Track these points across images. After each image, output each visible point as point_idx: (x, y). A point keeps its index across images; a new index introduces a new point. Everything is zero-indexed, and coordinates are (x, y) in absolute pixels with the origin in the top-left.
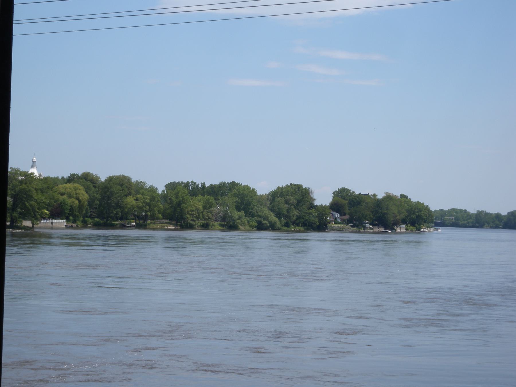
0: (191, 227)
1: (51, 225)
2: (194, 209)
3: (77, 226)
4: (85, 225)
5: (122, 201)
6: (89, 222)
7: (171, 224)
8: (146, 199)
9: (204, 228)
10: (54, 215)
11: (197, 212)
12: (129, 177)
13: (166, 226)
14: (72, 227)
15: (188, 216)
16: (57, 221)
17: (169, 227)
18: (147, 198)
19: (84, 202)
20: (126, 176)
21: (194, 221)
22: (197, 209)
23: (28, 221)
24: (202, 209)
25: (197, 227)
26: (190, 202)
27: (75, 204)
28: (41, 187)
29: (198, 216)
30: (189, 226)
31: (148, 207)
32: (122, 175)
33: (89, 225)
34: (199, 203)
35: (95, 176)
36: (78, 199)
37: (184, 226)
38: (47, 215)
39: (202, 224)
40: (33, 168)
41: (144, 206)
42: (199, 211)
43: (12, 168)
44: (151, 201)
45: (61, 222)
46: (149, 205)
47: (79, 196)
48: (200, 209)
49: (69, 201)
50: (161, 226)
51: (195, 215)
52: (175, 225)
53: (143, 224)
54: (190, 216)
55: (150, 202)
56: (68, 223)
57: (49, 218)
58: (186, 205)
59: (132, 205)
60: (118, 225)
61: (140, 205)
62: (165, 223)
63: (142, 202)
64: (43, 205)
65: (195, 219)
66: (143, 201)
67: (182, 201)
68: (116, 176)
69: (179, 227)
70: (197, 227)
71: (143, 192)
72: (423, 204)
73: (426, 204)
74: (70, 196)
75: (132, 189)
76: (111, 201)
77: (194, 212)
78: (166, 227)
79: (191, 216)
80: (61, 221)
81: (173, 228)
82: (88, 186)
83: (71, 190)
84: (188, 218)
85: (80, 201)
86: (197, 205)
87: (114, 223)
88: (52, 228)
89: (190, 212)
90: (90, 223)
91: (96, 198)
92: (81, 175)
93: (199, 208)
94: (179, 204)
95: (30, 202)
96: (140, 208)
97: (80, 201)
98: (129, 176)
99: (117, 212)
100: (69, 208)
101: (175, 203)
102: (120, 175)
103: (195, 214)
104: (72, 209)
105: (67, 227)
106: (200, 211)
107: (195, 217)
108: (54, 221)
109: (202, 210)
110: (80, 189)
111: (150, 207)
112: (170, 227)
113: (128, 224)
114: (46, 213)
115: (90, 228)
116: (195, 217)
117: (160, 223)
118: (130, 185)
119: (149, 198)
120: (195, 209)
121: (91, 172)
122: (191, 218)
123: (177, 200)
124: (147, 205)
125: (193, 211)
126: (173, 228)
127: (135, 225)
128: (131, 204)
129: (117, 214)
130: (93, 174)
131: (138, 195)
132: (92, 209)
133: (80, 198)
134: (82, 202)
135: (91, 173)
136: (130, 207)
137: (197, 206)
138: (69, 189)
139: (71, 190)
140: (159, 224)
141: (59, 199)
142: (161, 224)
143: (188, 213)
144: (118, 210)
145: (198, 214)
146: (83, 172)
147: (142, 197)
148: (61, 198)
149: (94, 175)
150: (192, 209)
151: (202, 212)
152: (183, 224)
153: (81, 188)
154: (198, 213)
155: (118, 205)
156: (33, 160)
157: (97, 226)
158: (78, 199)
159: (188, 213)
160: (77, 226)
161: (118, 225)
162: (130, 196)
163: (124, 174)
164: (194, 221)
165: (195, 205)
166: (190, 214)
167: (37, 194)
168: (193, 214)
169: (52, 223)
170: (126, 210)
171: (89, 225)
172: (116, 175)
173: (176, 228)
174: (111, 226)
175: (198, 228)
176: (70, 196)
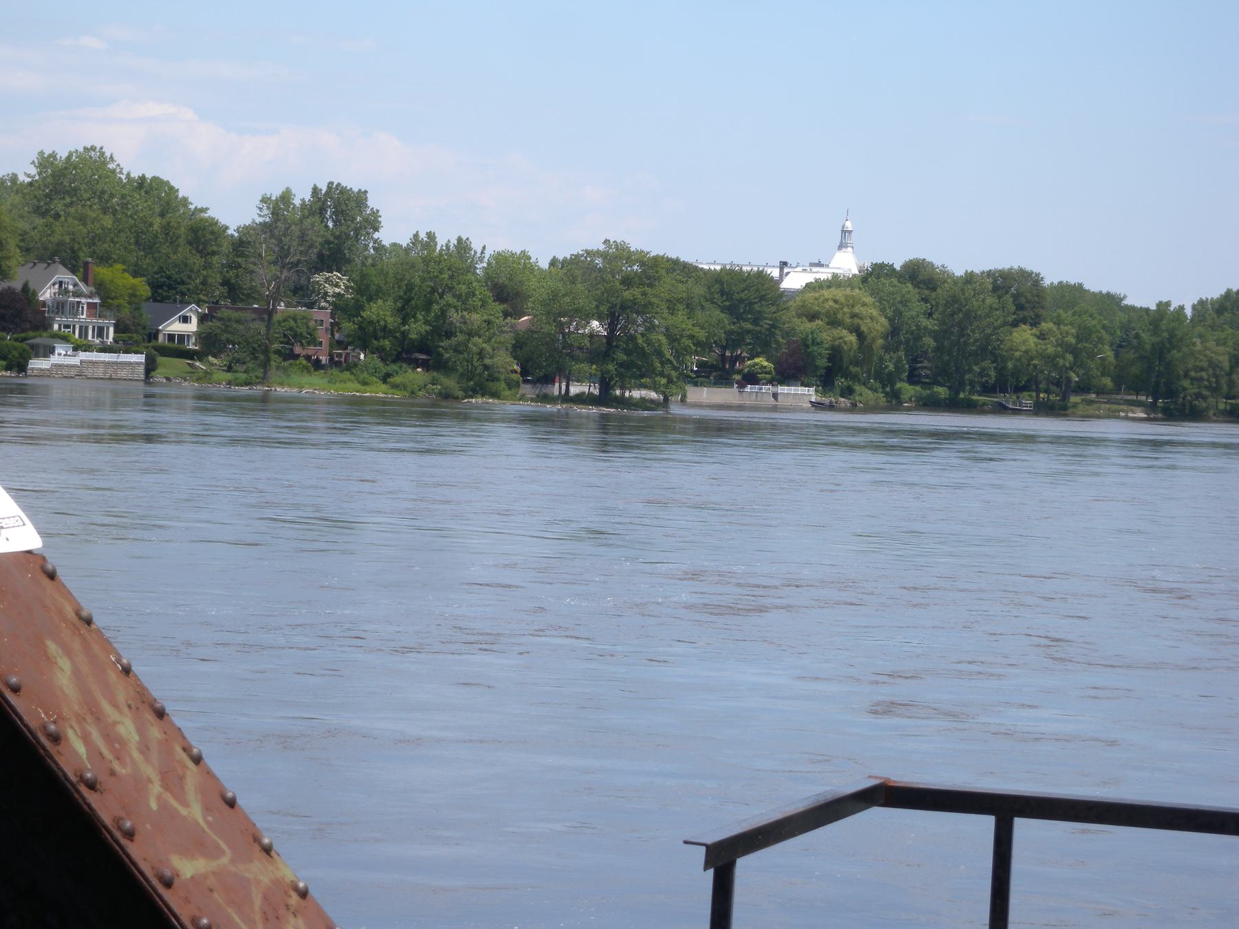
0: (1194, 414)
1: (772, 399)
2: (1205, 364)
3: (854, 405)
4: (894, 402)
5: (998, 340)
6: (905, 396)
7: (1139, 404)
8: (1064, 335)
9: (1230, 419)
10: (786, 374)
11: (1211, 372)
12: (1038, 275)
13: (1123, 412)
14: (831, 407)
15: (1186, 383)
16: (791, 390)
17: (1130, 415)
18: (1067, 333)
19: (874, 340)
20: (1027, 272)
21: (1205, 398)
22: (1213, 365)
23: (705, 389)
24: (1226, 365)
25: (1214, 414)
26: (1194, 344)
27: (845, 343)
28: (684, 295)
29: (1214, 385)
30: (1187, 411)
31: (1070, 357)
32: (1016, 267)
33: (906, 403)
34: (1221, 349)
35: (941, 270)
36: (857, 331)
37: (1174, 412)
38: (766, 373)
39: (1228, 407)
40: (844, 250)
41: (1057, 356)
42: (1218, 370)
43: (609, 241)
44: (1079, 338)
45: (801, 394)
46: (1074, 351)
47: (861, 322)
48: (1220, 365)
49: (827, 336)
50: (1109, 409)
51: (1206, 383)
52: (1152, 407)
53: (1061, 403)
54: (1192, 384)
55: (1077, 343)
56: (828, 395)
57: (770, 382)
58: (1181, 354)
59: (1026, 352)
60: (987, 405)
61: (1049, 351)
62: (1122, 402)
63: (1055, 343)
64: (689, 343)
65: (1205, 393)
66: (1056, 341)
67: (1170, 343)
68: (1000, 271)
69: (1160, 415)
70: (1214, 414)
71: (1059, 315)
72: (1101, 292)
73: (1104, 291)
74: (834, 322)
75: (1042, 308)
76: (966, 337)
77: (1204, 374)
78: (1122, 414)
79: (1195, 383)
80: (794, 390)
81: (1143, 415)
82: (903, 296)
83: (837, 306)
84: (1185, 389)
85: (861, 336)
86: (1212, 355)
87: (977, 400)
88: (775, 409)
89: (1193, 374)
90: (910, 399)
91: (926, 328)
92: (902, 267)
93: (1219, 361)
94: (1160, 351)
95: (648, 336)
96: (1051, 360)
97: (861, 336)
98: (1035, 270)
99: (983, 369)
100: (828, 354)
101: (1148, 347)
102: (1011, 269)
103: (1208, 380)
104: (836, 353)
105: (817, 406)
106: (1221, 369)
107: (1206, 387)
108: (782, 389)
109: (1227, 368)
110: (864, 305)
111: (1075, 357)
112: (1135, 413)
113: (1014, 403)
114: (765, 367)
115: (909, 409)
116: (1206, 387)
117: (1108, 402)
118: (1037, 296)
119: (1073, 331)
120: (1207, 363)
121: (929, 259)
122: (1196, 390)
123: (1156, 339)
124: (1067, 351)
125: (1202, 369)
126: (1143, 415)
127: (1030, 407)
128: (1023, 348)
129: (983, 373)
130: (933, 265)
131: (1043, 324)
132: (926, 362)
133: (864, 328)
134: (869, 340)
135: (929, 263)
136: (1021, 357)
137: (1212, 357)
138: (831, 303)
139: (837, 306)
140: (1103, 406)
141: (793, 329)
142: (1108, 406)
143: (1186, 375)
144: (987, 363)
145: (1214, 380)
146: (907, 260)
147: (1055, 328)
148: (806, 326)
149: (938, 268)
150: (1197, 363)
151: (1229, 374)
152: (1171, 407)
153: (869, 300)
154: (1216, 376)
155: (987, 350)
156: (843, 227)
157: (930, 404)
158: (857, 331)
159: (1186, 375)
160: (854, 405)
161: (987, 405)
162: (1024, 326)
163: (1023, 266)
164: (1205, 398)
165: (1208, 352)
166: (1193, 379)
167: (672, 314)
168: (1202, 379)
169: (775, 396)
170: (1010, 365)
171: (906, 404)
172: (1000, 267)
173: (1152, 416)
174: (969, 407)
175: (1214, 418)
176: (834, 322)
